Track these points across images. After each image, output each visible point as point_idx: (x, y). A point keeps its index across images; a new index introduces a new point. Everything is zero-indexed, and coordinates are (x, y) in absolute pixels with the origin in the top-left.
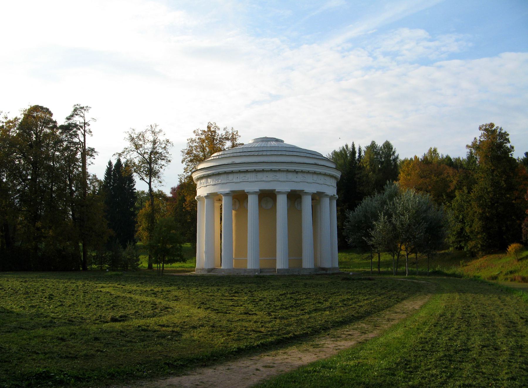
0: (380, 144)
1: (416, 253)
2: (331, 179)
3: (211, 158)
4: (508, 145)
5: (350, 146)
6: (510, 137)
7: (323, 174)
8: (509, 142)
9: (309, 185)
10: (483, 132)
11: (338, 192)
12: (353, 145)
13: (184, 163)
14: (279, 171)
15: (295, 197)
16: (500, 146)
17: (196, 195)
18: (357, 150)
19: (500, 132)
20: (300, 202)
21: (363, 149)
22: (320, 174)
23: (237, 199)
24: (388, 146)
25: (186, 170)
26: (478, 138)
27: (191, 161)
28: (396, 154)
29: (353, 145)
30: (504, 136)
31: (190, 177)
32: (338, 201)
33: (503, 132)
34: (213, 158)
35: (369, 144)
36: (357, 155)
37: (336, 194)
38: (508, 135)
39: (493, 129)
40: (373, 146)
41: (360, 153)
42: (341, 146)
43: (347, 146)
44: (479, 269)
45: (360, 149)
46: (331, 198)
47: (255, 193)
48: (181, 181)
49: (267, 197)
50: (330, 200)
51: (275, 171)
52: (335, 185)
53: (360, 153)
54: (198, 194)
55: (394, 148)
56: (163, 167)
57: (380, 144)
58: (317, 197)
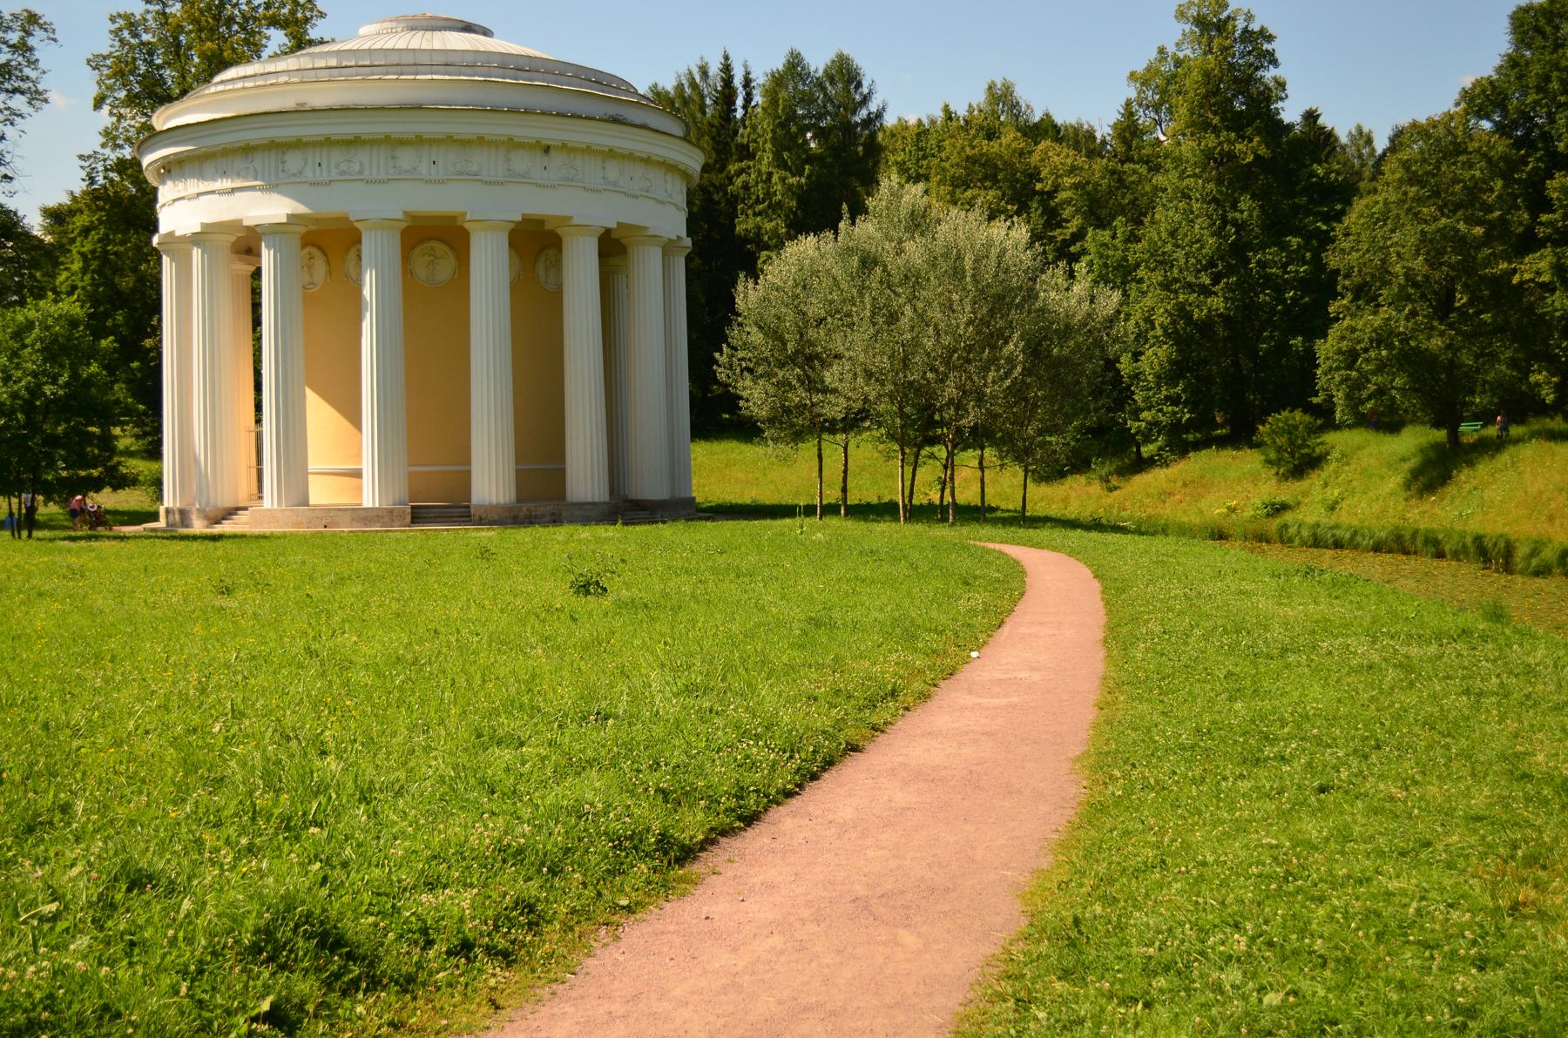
0: (817, 62)
1: (982, 449)
2: (669, 178)
3: (213, 90)
4: (1269, 74)
5: (715, 69)
6: (1278, 47)
7: (642, 160)
8: (1274, 62)
9: (583, 205)
10: (1187, 28)
11: (690, 232)
12: (727, 68)
13: (106, 109)
14: (481, 141)
15: (536, 244)
16: (1244, 81)
17: (155, 229)
18: (738, 82)
19: (1245, 30)
20: (557, 264)
21: (760, 78)
22: (630, 157)
23: (314, 245)
24: (845, 73)
25: (110, 137)
26: (1171, 49)
27: (132, 100)
28: (873, 107)
29: (727, 68)
30: (1258, 43)
31: (129, 168)
32: (688, 259)
33: (1255, 26)
34: (220, 88)
35: (779, 64)
36: (740, 102)
37: (683, 233)
38: (1270, 38)
39: (1223, 16)
40: (795, 65)
41: (748, 98)
42: (683, 70)
43: (704, 72)
44: (1165, 495)
45: (747, 83)
46: (668, 248)
47: (385, 224)
48: (92, 180)
49: (434, 241)
50: (664, 254)
51: (464, 143)
52: (681, 200)
53: (748, 98)
54: (165, 226)
55: (866, 83)
56: (18, 120)
57: (817, 62)
58: (613, 248)
